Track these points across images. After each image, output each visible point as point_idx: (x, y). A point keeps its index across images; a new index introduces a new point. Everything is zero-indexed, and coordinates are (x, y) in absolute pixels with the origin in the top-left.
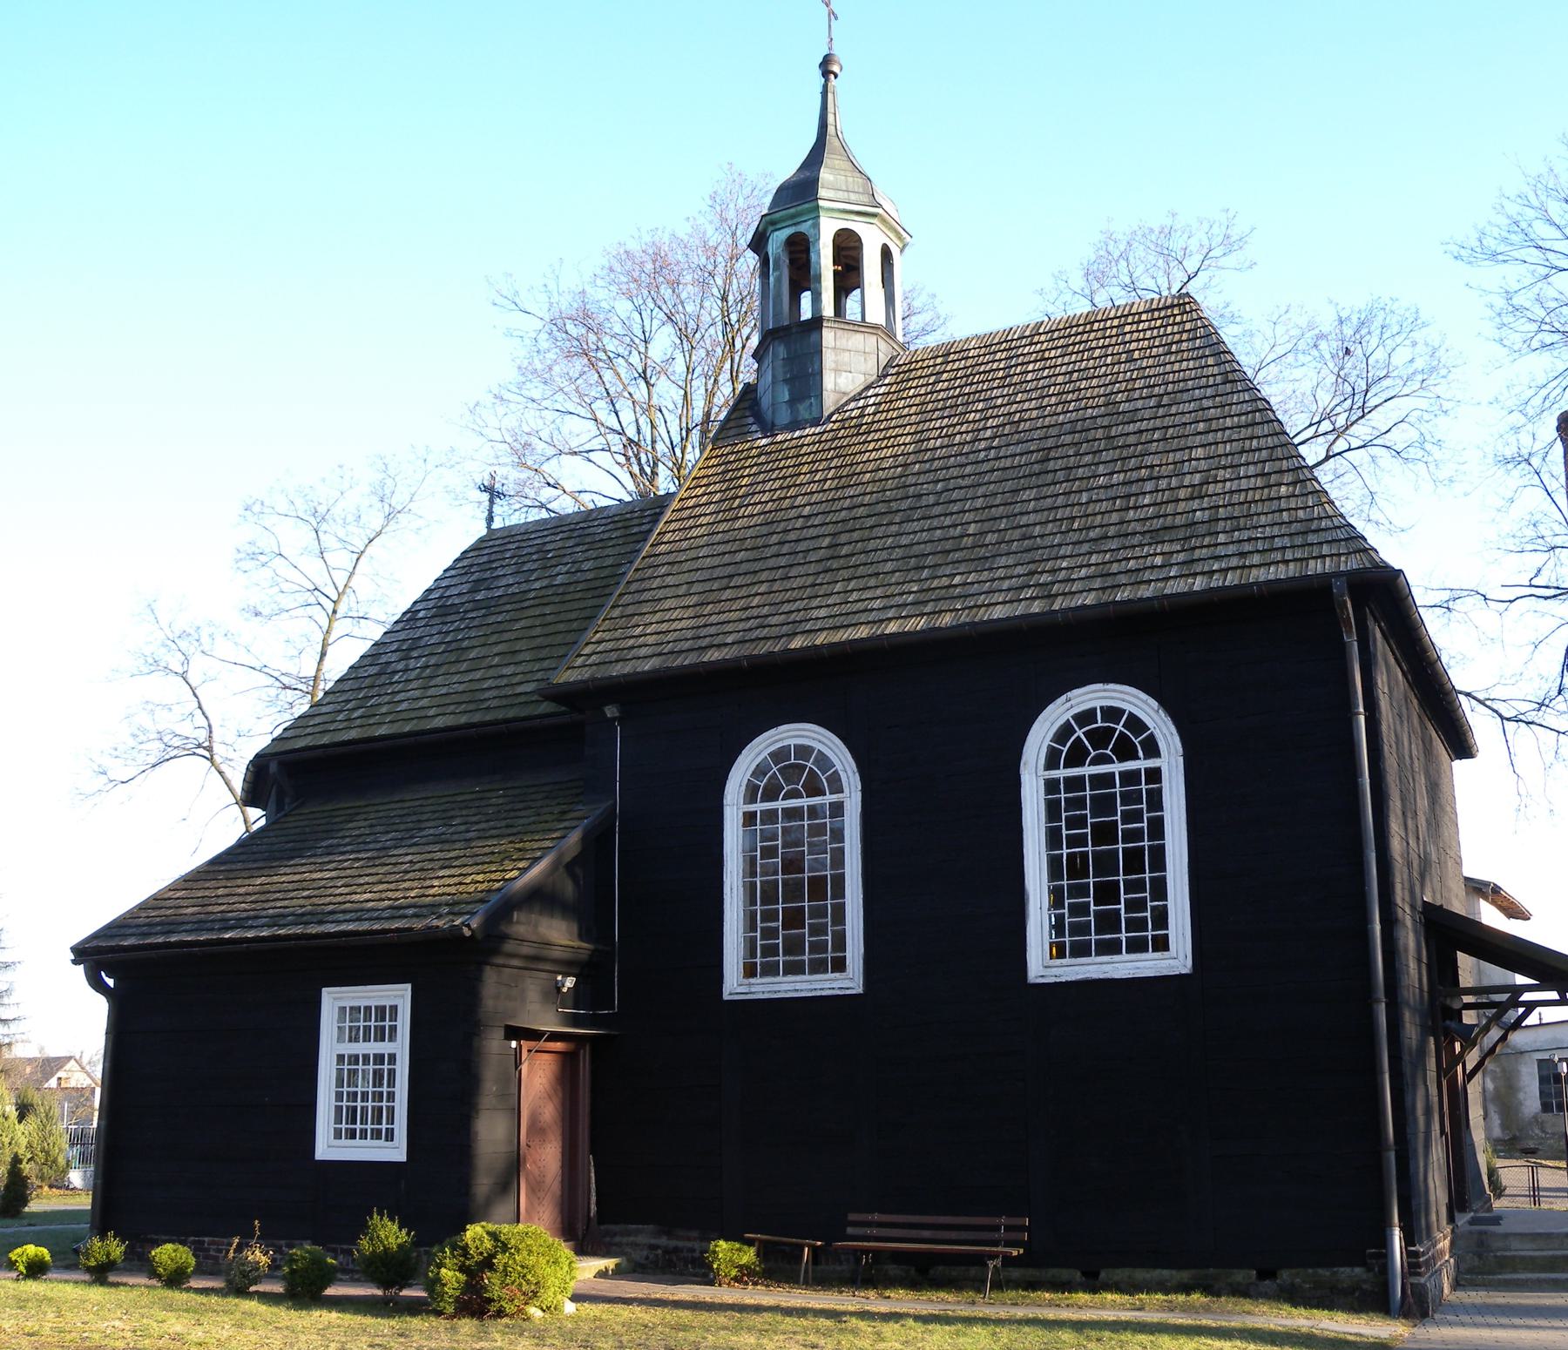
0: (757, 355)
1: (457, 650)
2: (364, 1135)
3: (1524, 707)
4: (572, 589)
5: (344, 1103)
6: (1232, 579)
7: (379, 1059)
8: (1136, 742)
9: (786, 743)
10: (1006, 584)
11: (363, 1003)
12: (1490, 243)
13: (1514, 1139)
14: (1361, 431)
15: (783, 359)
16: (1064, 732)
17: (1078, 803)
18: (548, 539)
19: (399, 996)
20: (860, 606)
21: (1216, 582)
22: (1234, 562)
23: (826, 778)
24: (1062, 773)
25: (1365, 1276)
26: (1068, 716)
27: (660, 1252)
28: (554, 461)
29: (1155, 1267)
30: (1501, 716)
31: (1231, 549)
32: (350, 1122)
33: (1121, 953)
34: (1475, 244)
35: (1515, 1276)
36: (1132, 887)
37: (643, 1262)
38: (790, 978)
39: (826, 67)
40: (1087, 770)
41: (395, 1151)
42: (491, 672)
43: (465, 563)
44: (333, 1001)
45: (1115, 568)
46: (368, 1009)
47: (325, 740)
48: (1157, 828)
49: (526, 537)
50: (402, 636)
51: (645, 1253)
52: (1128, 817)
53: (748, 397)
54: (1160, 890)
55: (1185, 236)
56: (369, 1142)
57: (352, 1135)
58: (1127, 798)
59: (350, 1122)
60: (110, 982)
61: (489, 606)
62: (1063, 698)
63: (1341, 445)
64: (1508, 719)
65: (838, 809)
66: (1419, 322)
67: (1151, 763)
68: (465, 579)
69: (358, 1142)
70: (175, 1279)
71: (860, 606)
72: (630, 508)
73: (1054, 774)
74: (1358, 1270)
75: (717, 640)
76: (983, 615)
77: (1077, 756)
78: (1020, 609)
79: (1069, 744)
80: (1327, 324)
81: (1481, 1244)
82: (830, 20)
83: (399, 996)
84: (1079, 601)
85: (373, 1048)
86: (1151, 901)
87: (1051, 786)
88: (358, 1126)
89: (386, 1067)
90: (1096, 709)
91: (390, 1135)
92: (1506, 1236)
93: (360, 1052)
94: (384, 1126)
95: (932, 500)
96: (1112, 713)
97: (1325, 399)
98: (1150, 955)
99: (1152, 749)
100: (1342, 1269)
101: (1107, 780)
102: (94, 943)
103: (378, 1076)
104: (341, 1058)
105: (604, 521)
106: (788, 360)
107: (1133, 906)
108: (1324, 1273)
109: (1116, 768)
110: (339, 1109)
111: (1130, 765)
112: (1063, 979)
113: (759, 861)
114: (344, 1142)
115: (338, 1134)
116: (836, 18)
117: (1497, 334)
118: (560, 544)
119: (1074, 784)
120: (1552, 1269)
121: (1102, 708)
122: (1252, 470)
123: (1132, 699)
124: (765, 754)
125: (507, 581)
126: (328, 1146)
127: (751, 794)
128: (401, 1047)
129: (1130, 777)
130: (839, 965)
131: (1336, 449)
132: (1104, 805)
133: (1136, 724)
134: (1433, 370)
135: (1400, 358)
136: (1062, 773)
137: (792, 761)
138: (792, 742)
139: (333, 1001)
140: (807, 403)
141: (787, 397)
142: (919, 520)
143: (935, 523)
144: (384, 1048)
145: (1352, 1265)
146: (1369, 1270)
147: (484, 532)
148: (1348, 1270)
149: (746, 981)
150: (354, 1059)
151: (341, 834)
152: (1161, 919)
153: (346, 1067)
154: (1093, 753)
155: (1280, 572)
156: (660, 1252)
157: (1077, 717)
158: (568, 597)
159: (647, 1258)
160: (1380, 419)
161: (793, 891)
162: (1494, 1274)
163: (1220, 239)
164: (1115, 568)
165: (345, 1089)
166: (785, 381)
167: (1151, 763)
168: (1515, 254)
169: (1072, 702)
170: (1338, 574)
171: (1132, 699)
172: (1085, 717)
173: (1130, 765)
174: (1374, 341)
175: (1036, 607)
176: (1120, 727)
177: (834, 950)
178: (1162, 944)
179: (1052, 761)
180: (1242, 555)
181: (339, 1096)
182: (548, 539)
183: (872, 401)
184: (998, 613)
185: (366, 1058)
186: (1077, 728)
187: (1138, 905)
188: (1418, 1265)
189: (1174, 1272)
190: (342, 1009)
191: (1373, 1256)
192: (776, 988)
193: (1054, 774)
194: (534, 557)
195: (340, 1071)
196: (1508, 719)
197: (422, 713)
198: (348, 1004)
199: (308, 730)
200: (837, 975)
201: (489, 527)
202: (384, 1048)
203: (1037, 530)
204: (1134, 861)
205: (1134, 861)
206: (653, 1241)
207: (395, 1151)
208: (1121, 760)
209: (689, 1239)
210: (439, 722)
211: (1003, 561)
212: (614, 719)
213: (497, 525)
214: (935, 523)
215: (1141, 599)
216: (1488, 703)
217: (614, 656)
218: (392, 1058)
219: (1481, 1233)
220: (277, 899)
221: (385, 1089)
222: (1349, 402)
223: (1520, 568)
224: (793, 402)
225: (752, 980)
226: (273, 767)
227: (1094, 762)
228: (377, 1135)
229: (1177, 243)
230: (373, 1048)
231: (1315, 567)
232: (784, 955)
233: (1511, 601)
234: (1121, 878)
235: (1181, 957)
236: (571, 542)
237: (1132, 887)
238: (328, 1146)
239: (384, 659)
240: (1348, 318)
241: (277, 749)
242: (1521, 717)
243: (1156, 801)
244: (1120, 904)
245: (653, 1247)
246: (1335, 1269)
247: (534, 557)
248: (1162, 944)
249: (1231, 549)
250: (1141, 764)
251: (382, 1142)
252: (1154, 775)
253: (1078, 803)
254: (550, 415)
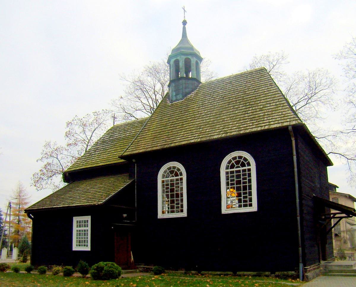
0: (169, 86)
1: (105, 149)
2: (82, 246)
3: (352, 156)
4: (130, 136)
5: (78, 239)
6: (266, 127)
7: (85, 231)
8: (245, 163)
9: (170, 166)
10: (217, 131)
11: (81, 220)
12: (344, 54)
13: (353, 248)
14: (314, 98)
15: (174, 86)
16: (230, 162)
17: (233, 176)
18: (126, 127)
19: (88, 218)
20: (187, 137)
21: (263, 128)
22: (268, 124)
23: (179, 173)
24: (229, 170)
25: (294, 273)
26: (231, 158)
27: (145, 269)
28: (136, 112)
29: (249, 271)
30: (347, 158)
31: (267, 121)
32: (80, 243)
33: (247, 207)
34: (340, 54)
35: (333, 274)
36: (244, 193)
37: (142, 270)
38: (172, 214)
39: (185, 23)
40: (235, 169)
41: (88, 249)
42: (112, 154)
43: (109, 132)
44: (75, 219)
45: (241, 126)
46: (82, 221)
47: (78, 168)
48: (250, 181)
49: (121, 126)
50: (95, 147)
51: (142, 269)
52: (244, 179)
53: (168, 95)
54: (250, 194)
55: (273, 57)
56: (83, 247)
57: (80, 245)
58: (244, 175)
59: (80, 243)
60: (33, 217)
61: (112, 141)
62: (230, 154)
63: (310, 101)
64: (349, 159)
65: (181, 179)
66: (328, 73)
67: (249, 167)
68: (108, 135)
69: (81, 247)
70: (267, 276)
71: (187, 137)
72: (143, 120)
73: (228, 170)
74: (293, 272)
75: (156, 145)
76: (212, 138)
77: (232, 167)
78: (220, 136)
79: (231, 164)
80: (306, 74)
81: (326, 267)
82: (184, 12)
83: (88, 218)
84: (233, 134)
85: (84, 228)
86: (247, 196)
87: (227, 173)
88: (81, 244)
89: (86, 232)
90: (236, 157)
91: (87, 246)
92: (331, 266)
93: (86, 229)
94: (86, 244)
95: (204, 114)
96: (240, 157)
97: (306, 91)
98: (248, 207)
99: (249, 164)
100: (289, 272)
101: (239, 171)
102: (29, 209)
103: (85, 234)
104: (77, 231)
105: (137, 122)
106: (175, 86)
107: (244, 197)
108: (286, 272)
109: (241, 169)
110: (77, 241)
111: (244, 168)
112: (229, 213)
113: (165, 190)
114: (78, 247)
115: (77, 246)
116: (186, 12)
117: (346, 75)
118: (128, 128)
119: (232, 172)
120: (341, 272)
121: (238, 156)
122: (274, 104)
123: (245, 154)
124: (166, 168)
125: (117, 135)
126: (75, 248)
127: (163, 176)
128: (89, 228)
129: (244, 171)
130: (182, 211)
131: (309, 102)
132: (238, 176)
133: (245, 159)
134: (331, 84)
135: (323, 81)
136: (229, 170)
137: (172, 170)
138: (172, 166)
139: (75, 219)
140: (179, 96)
141: (175, 94)
142: (200, 118)
143: (204, 119)
144: (86, 228)
145: (292, 271)
146: (296, 272)
147: (113, 126)
148: (291, 272)
149: (163, 214)
150: (80, 231)
151: (80, 187)
152: (251, 200)
153: (78, 232)
154: (236, 166)
155: (278, 125)
156: (145, 269)
157: (233, 158)
158: (129, 138)
159: (143, 270)
160: (319, 95)
161: (172, 196)
162: (328, 273)
163: (281, 57)
164: (241, 126)
165: (78, 237)
166: (174, 91)
167: (249, 167)
168: (350, 56)
169: (232, 155)
170: (290, 125)
171: (245, 154)
172: (234, 158)
173: (244, 168)
174: (317, 78)
175: (223, 135)
176: (242, 160)
177: (181, 208)
178: (251, 205)
179: (227, 168)
180: (269, 122)
181: (77, 238)
182: (126, 127)
183: (193, 94)
184: (215, 137)
185: (82, 230)
186: (232, 160)
187: (246, 197)
188: (307, 271)
189: (252, 272)
190: (77, 221)
191: (296, 269)
192: (173, 215)
193: (228, 170)
194: (123, 130)
195: (77, 233)
196: (349, 159)
197: (97, 163)
198: (78, 220)
199: (75, 167)
200: (181, 213)
201: (114, 125)
202: (86, 228)
203: (226, 119)
204: (245, 188)
205: (245, 188)
206: (144, 266)
207: (88, 249)
208: (242, 167)
209: (152, 266)
210: (101, 164)
211: (218, 126)
212: (134, 162)
213: (115, 124)
214: (204, 119)
215: (246, 133)
216: (344, 156)
217: (135, 149)
218: (87, 230)
219: (326, 265)
220: (66, 200)
221: (86, 236)
222: (311, 92)
223: (349, 126)
224: (176, 95)
225: (164, 214)
226: (67, 174)
227: (237, 168)
228: (85, 245)
229: (271, 59)
230: (84, 228)
231: (285, 124)
232: (171, 209)
233: (348, 133)
234: (242, 192)
235: (255, 207)
236: (130, 127)
237: (244, 193)
238: (75, 248)
239: (91, 152)
240: (311, 73)
241: (68, 171)
242: (352, 159)
243: (250, 175)
244: (241, 197)
245: (144, 268)
246: (288, 272)
247: (123, 130)
248: (251, 205)
249: (267, 121)
250: (246, 168)
251: (86, 247)
252: (249, 170)
253: (233, 176)
254: (133, 102)
